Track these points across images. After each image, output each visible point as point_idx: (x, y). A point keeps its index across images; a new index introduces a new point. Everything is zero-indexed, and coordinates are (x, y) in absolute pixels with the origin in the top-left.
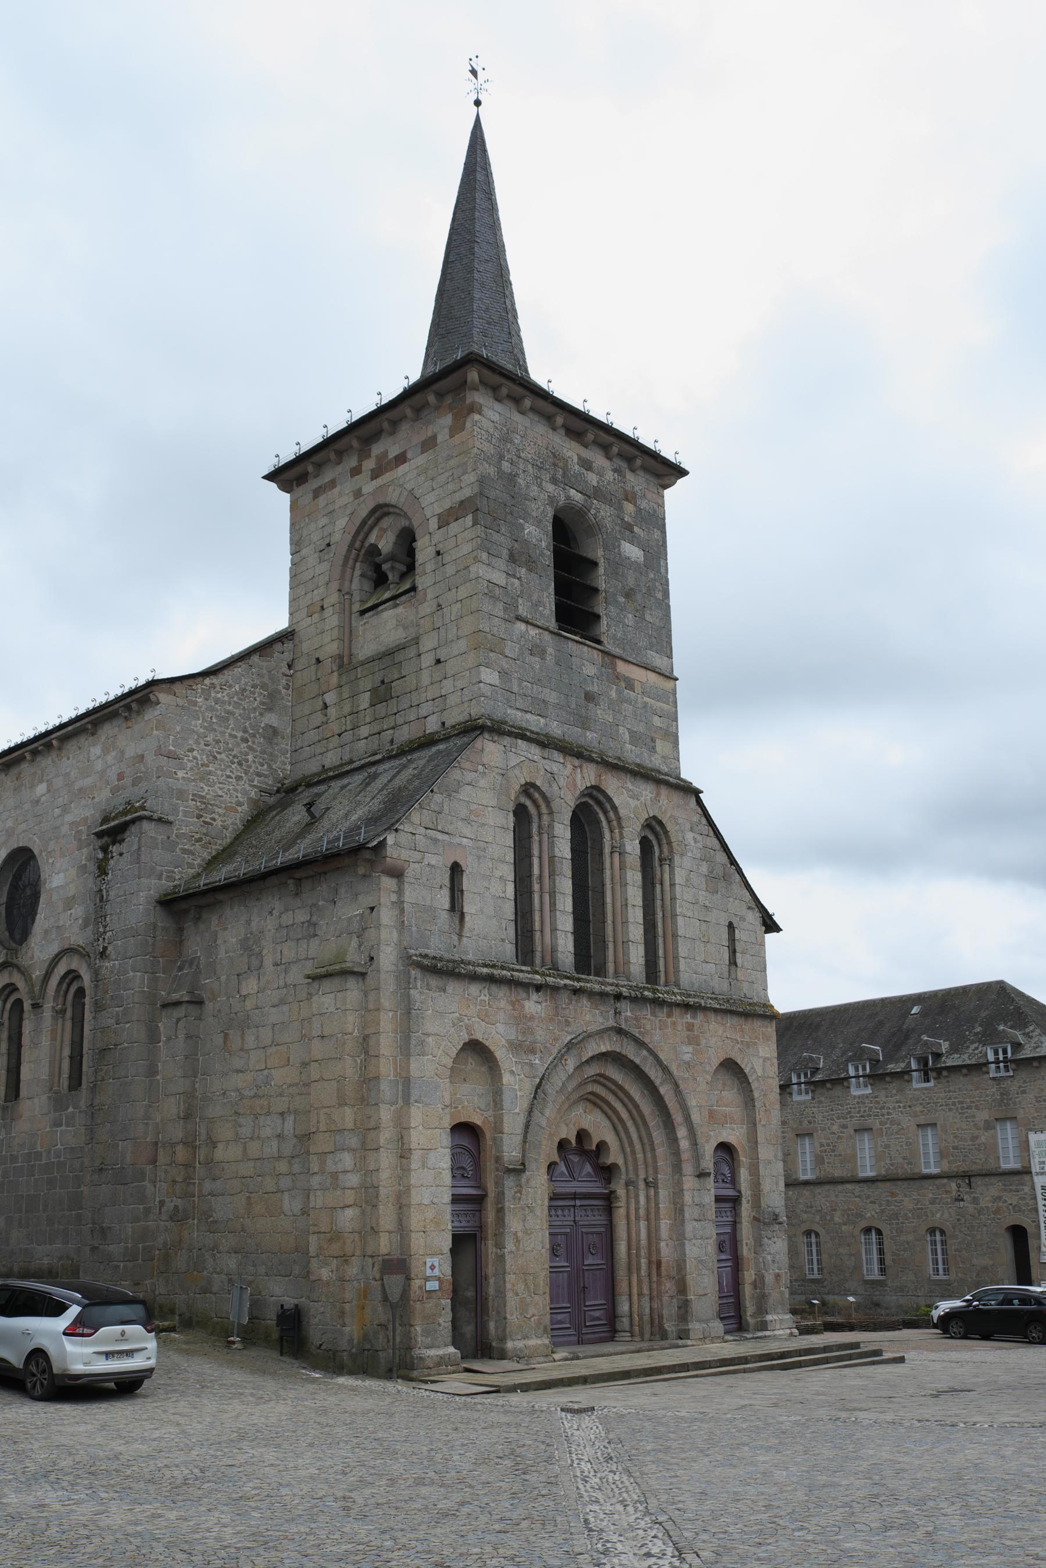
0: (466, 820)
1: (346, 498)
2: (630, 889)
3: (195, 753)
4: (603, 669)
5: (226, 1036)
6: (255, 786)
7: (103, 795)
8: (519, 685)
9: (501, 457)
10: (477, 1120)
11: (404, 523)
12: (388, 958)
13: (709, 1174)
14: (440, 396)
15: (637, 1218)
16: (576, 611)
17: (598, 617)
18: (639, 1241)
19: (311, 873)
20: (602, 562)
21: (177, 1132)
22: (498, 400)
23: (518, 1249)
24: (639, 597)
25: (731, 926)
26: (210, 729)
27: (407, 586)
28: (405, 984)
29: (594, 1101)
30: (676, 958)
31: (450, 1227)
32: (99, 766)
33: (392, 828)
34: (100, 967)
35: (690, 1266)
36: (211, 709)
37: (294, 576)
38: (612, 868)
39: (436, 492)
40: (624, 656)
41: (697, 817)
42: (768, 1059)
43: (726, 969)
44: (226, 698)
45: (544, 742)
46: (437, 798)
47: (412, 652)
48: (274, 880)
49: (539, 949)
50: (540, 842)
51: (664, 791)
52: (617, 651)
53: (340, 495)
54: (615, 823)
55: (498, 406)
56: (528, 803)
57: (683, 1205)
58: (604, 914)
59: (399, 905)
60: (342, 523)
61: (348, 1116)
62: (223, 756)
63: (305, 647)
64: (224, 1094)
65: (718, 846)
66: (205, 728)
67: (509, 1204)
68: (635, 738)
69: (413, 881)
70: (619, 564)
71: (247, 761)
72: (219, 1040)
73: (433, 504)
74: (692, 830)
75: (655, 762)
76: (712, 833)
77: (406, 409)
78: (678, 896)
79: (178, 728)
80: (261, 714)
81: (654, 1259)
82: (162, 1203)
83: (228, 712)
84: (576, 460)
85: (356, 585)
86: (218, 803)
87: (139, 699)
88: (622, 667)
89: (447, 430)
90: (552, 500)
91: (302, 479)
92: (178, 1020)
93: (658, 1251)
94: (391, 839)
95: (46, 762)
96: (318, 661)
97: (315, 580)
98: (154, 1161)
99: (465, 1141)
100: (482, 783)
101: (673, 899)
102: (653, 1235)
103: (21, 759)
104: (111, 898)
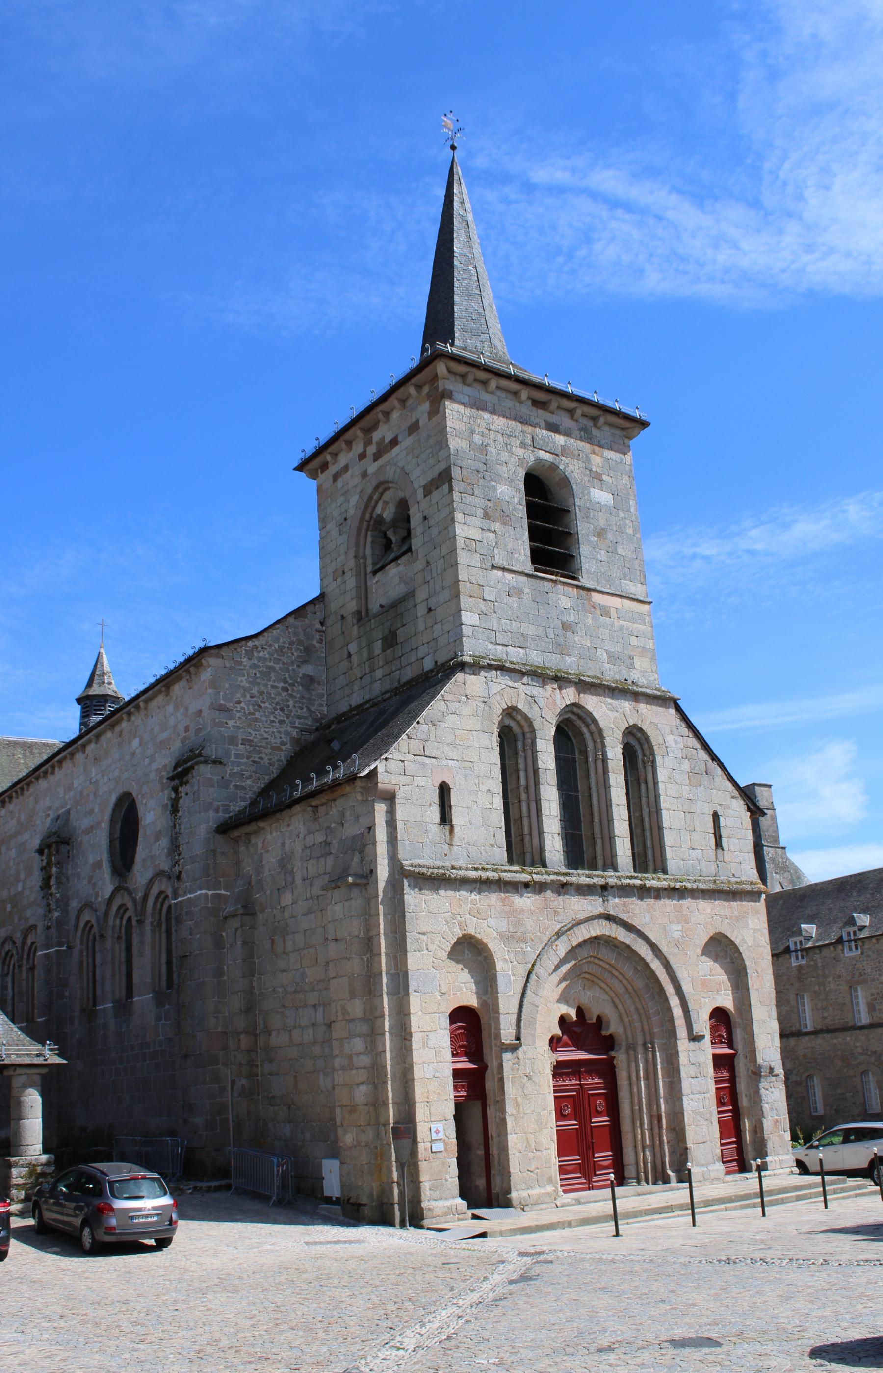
1: (355, 472)
3: (243, 705)
4: (579, 601)
5: (273, 941)
6: (296, 727)
7: (176, 746)
8: (499, 624)
9: (472, 432)
11: (401, 494)
13: (703, 1037)
19: (323, 801)
21: (240, 1023)
23: (518, 1112)
24: (610, 535)
25: (716, 816)
26: (254, 683)
27: (405, 548)
32: (172, 721)
34: (178, 888)
36: (254, 666)
37: (322, 548)
38: (596, 773)
40: (598, 588)
42: (759, 930)
43: (712, 853)
44: (267, 656)
46: (424, 728)
50: (525, 757)
53: (352, 477)
55: (467, 390)
56: (513, 724)
60: (354, 500)
61: (357, 1008)
62: (267, 705)
63: (333, 606)
64: (274, 990)
66: (250, 682)
68: (613, 658)
69: (405, 801)
71: (289, 706)
72: (268, 945)
74: (672, 733)
77: (356, 431)
79: (227, 685)
80: (299, 666)
82: (233, 1083)
83: (270, 667)
85: (368, 551)
86: (264, 744)
87: (193, 663)
89: (426, 415)
90: (521, 461)
92: (237, 929)
96: (343, 617)
98: (225, 1048)
104: (182, 831)
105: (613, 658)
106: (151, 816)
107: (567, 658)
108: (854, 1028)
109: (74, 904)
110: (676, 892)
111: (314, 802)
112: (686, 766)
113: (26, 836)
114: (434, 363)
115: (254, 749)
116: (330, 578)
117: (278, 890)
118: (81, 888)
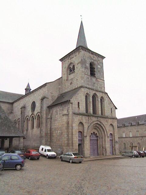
0: (80, 97)
1: (67, 62)
10: (81, 131)
12: (71, 113)
14: (77, 50)
16: (93, 74)
22: (83, 50)
28: (73, 116)
29: (95, 129)
33: (71, 98)
35: (107, 147)
45: (89, 88)
46: (76, 95)
51: (103, 94)
59: (72, 107)
60: (67, 65)
63: (63, 79)
67: (85, 140)
70: (98, 68)
73: (76, 62)
77: (68, 55)
87: (45, 85)
88: (98, 80)
91: (63, 60)
94: (71, 100)
95: (36, 92)
99: (80, 133)
100: (82, 93)
102: (102, 144)
103: (33, 92)
105: (100, 88)
106: (38, 105)
108: (130, 137)
109: (25, 116)
110: (23, 136)
112: (108, 102)
113: (18, 107)
116: (63, 75)
118: (26, 114)
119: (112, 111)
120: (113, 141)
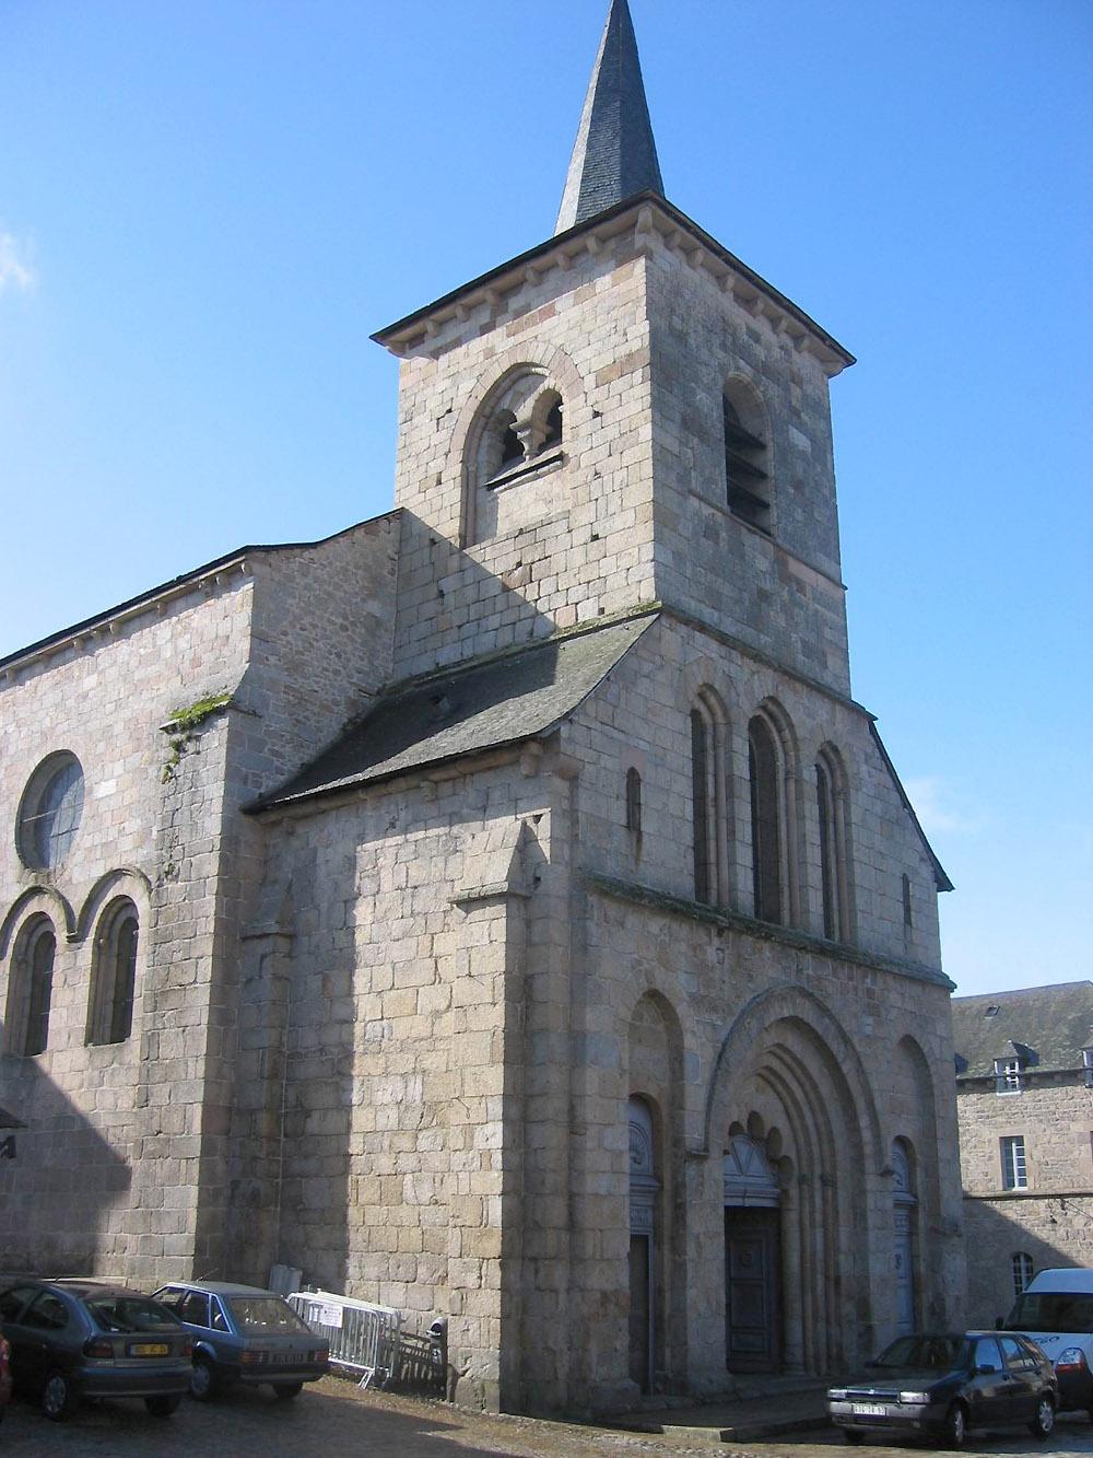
2: (808, 822)
3: (289, 638)
10: (652, 1090)
14: (603, 240)
15: (813, 1226)
17: (766, 506)
18: (814, 1254)
20: (770, 445)
28: (578, 917)
30: (853, 911)
31: (628, 1225)
38: (787, 797)
39: (594, 346)
41: (871, 748)
47: (561, 527)
48: (402, 783)
49: (714, 885)
50: (715, 756)
52: (786, 546)
54: (790, 744)
57: (865, 1211)
58: (777, 853)
60: (467, 385)
62: (320, 644)
65: (890, 784)
70: (786, 450)
75: (827, 678)
76: (885, 769)
78: (855, 837)
81: (832, 1274)
83: (328, 594)
84: (744, 330)
92: (263, 957)
93: (837, 1264)
97: (432, 450)
100: (661, 677)
101: (849, 841)
107: (762, 637)
111: (436, 776)
114: (637, 208)
115: (299, 703)
117: (345, 902)
119: (908, 909)
120: (922, 1221)
